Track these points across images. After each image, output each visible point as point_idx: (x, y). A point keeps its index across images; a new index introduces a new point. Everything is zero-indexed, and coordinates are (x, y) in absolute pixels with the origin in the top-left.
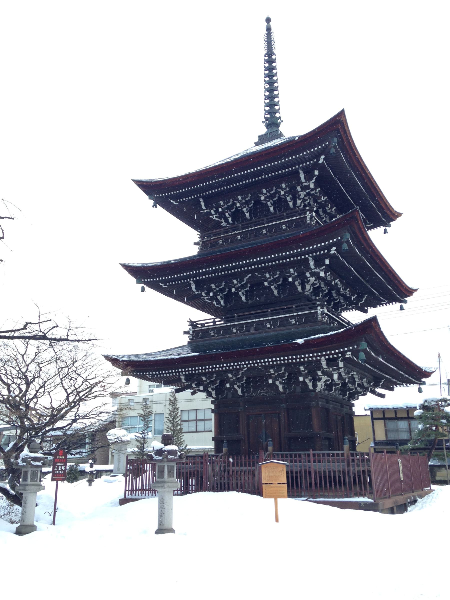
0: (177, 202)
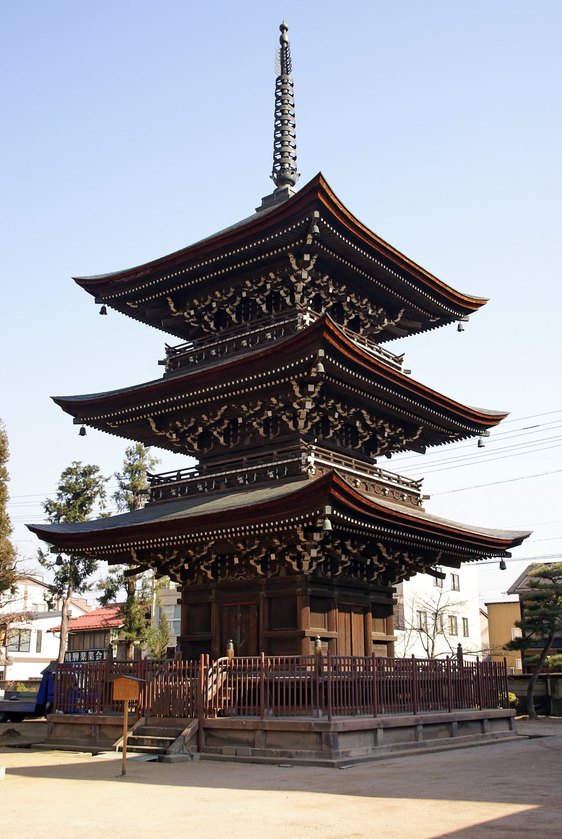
0: (136, 305)
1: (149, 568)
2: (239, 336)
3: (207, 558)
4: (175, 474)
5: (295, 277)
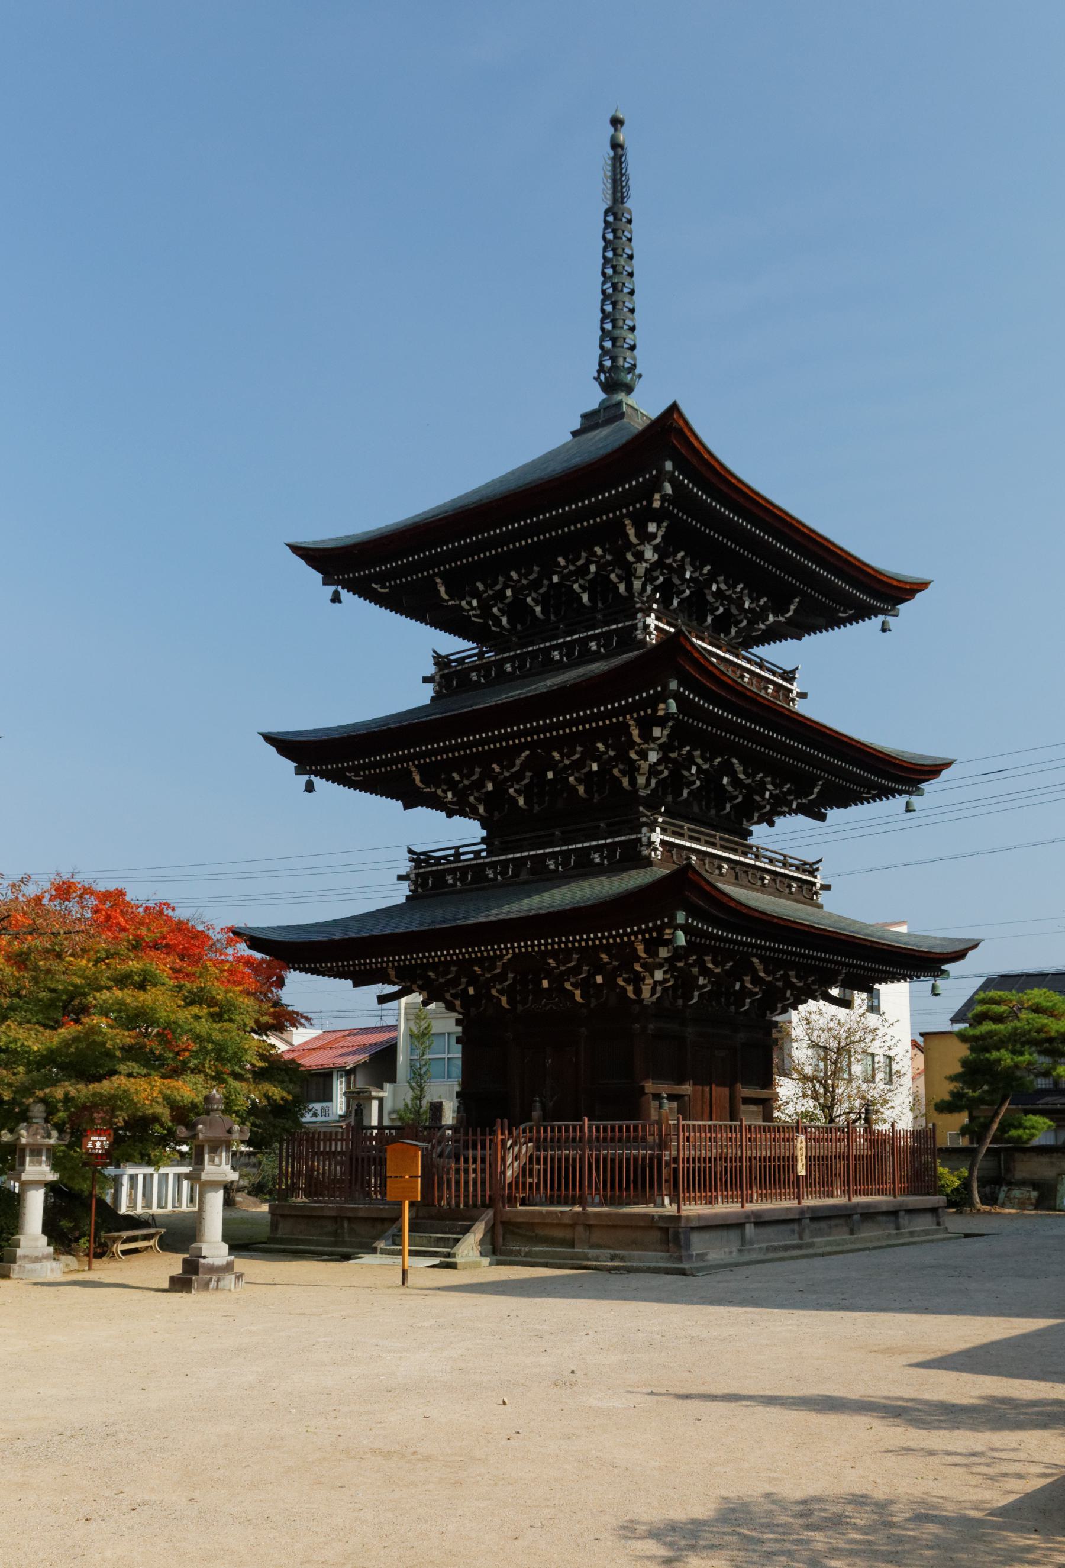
1: (413, 992)
2: (548, 644)
3: (502, 977)
4: (452, 852)
5: (633, 555)
